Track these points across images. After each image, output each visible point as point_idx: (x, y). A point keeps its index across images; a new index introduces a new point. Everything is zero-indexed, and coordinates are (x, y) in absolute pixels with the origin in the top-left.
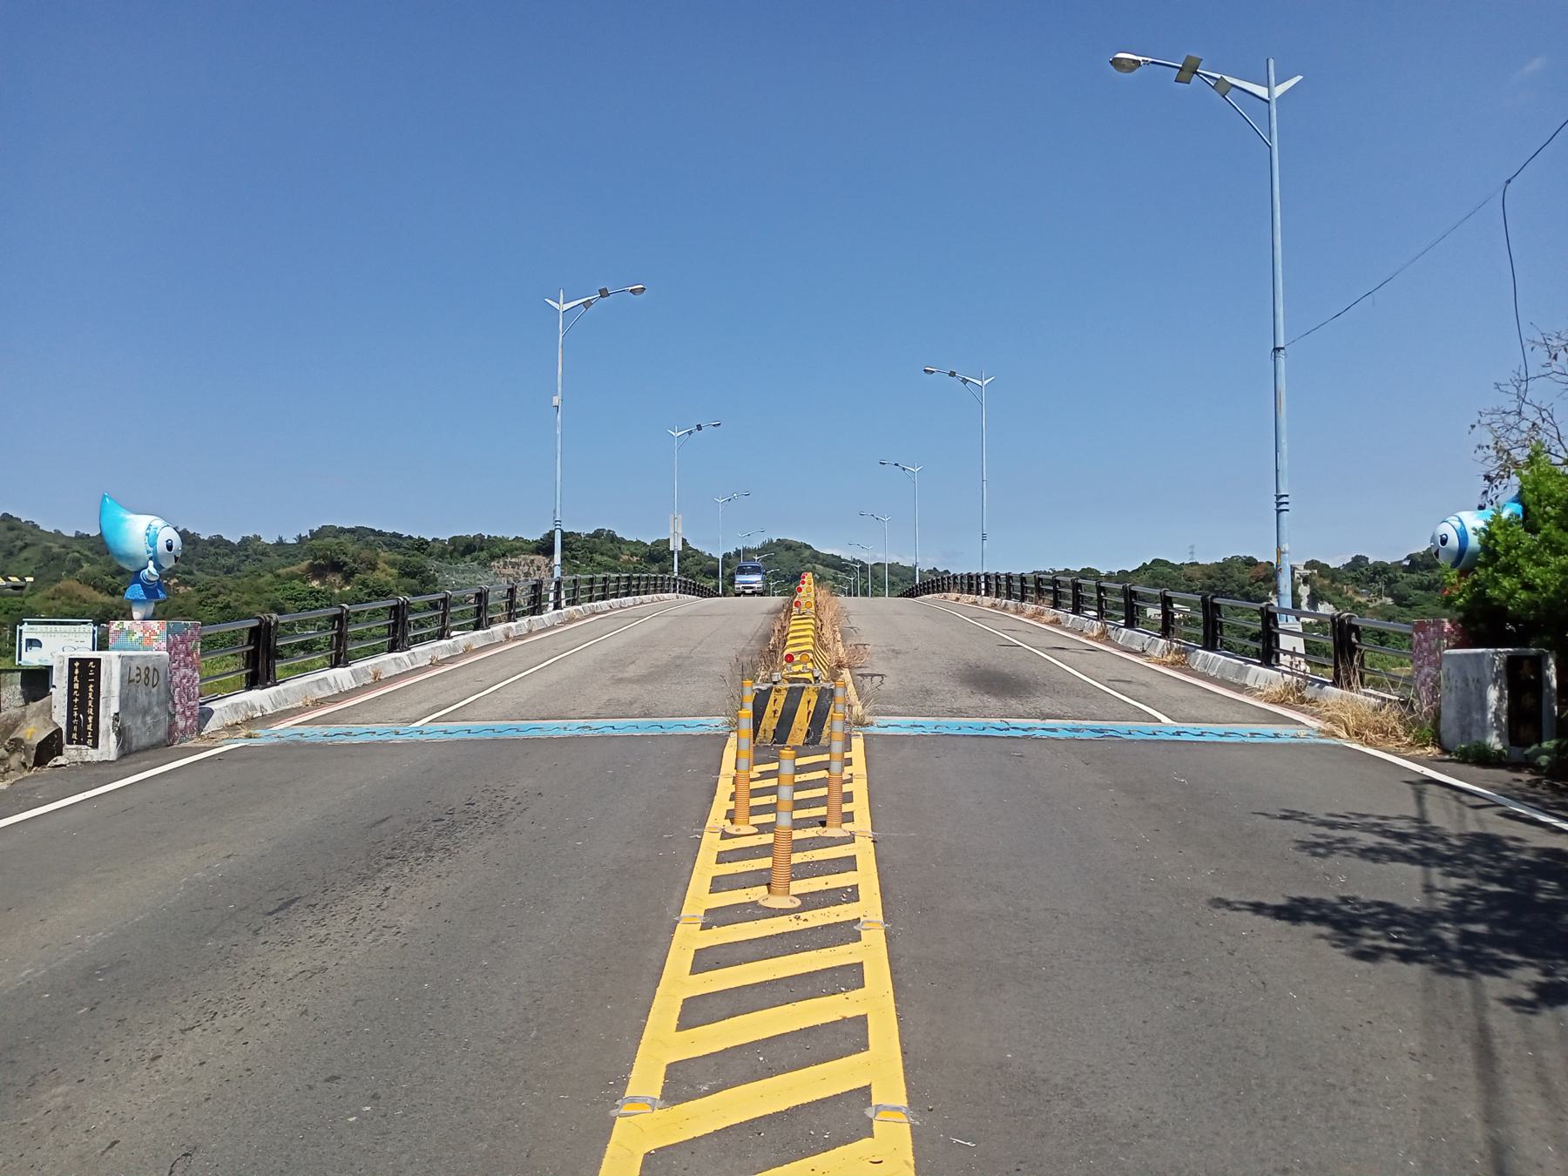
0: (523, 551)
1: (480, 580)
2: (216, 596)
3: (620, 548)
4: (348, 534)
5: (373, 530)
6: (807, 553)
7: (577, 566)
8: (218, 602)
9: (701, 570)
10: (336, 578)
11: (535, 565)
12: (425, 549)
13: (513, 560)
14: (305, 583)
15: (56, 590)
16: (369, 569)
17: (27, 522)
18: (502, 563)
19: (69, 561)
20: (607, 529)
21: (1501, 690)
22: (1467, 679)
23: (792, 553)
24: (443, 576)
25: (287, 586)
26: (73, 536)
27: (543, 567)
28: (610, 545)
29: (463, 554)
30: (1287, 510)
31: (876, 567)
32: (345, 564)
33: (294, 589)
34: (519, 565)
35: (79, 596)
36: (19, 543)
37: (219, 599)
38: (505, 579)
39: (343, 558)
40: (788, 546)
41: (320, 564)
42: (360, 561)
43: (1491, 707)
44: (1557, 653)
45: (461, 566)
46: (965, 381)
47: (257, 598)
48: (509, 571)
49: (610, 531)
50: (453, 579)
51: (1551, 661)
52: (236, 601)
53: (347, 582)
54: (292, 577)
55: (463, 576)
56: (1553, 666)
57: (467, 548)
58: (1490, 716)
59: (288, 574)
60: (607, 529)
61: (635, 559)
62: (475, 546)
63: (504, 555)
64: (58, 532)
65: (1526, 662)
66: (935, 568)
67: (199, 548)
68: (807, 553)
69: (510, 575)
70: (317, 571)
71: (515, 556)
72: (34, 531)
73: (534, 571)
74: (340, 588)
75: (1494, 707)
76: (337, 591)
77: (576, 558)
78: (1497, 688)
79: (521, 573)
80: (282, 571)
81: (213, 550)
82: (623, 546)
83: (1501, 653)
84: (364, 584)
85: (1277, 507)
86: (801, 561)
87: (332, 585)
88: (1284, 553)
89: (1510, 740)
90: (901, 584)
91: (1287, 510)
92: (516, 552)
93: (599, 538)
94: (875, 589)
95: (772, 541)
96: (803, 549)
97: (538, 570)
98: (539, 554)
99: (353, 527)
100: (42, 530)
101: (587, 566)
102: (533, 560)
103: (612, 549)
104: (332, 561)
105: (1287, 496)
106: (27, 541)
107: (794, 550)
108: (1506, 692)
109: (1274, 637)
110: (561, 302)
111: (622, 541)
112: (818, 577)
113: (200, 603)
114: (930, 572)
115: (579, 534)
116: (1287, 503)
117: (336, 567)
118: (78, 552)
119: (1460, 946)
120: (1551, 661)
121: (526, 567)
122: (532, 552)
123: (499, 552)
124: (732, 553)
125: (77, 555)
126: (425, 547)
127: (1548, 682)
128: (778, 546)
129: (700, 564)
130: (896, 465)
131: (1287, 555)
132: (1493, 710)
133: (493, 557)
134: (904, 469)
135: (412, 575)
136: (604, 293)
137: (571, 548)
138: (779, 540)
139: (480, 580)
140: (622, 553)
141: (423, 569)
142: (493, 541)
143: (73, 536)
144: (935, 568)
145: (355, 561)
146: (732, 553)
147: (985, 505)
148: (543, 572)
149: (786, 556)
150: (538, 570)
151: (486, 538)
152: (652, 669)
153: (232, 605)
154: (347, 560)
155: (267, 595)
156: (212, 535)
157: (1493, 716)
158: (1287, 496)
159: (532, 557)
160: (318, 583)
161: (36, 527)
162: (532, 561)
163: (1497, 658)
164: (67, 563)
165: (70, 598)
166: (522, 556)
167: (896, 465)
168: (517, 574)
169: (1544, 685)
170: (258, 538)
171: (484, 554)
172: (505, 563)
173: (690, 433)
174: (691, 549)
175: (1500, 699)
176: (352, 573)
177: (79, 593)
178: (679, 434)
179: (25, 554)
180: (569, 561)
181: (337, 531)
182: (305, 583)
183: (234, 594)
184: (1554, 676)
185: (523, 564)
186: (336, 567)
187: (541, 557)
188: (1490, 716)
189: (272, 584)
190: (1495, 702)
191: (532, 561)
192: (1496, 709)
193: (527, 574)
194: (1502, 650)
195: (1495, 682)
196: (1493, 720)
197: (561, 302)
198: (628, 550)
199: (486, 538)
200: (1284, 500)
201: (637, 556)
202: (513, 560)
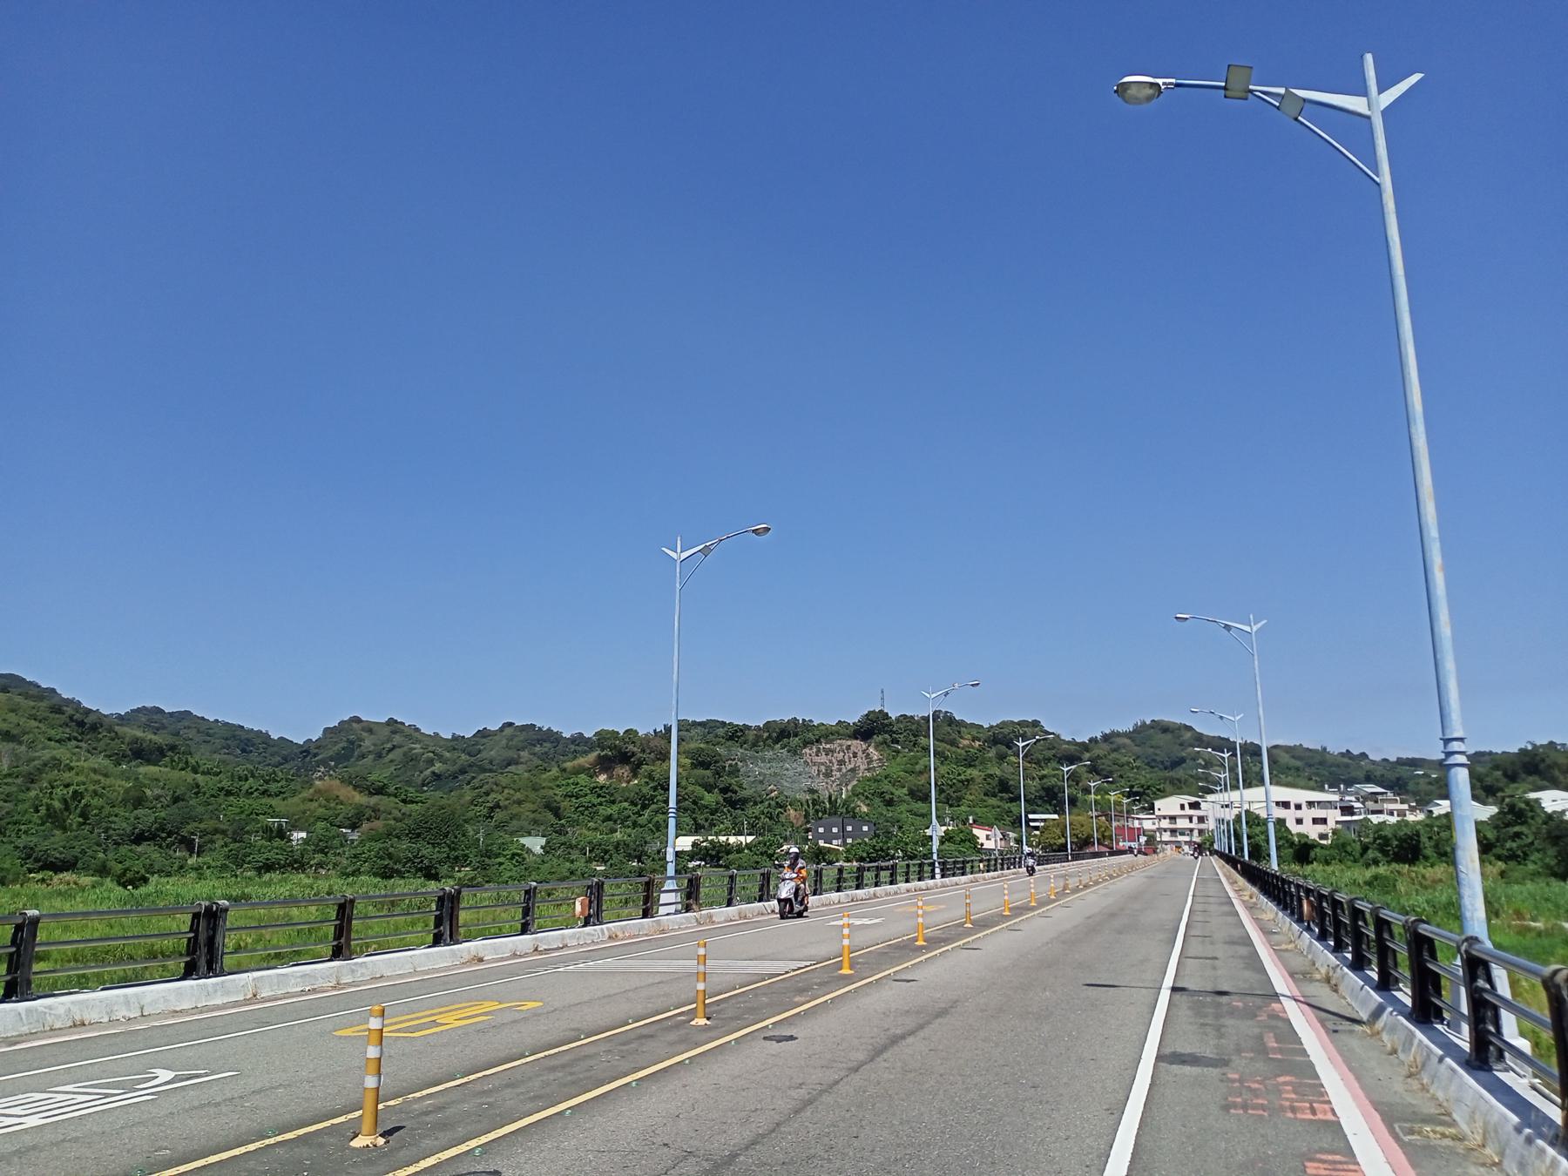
0: (840, 736)
1: (787, 770)
2: (487, 794)
3: (959, 732)
4: (699, 728)
6: (1188, 735)
7: (898, 752)
8: (488, 802)
9: (1054, 756)
10: (623, 771)
11: (851, 751)
12: (739, 737)
13: (828, 746)
14: (592, 777)
15: (315, 791)
16: (658, 759)
17: (409, 725)
18: (815, 750)
19: (424, 761)
20: (943, 711)
23: (1169, 736)
24: (747, 765)
25: (571, 781)
26: (450, 737)
27: (860, 753)
28: (949, 729)
29: (777, 741)
31: (1274, 751)
32: (633, 754)
33: (577, 784)
34: (833, 751)
35: (338, 797)
36: (389, 746)
37: (490, 798)
38: (816, 768)
39: (631, 747)
40: (1165, 728)
41: (606, 755)
42: (648, 751)
45: (769, 754)
47: (532, 795)
48: (823, 758)
49: (947, 712)
50: (756, 769)
52: (507, 799)
53: (635, 776)
54: (579, 771)
55: (769, 765)
57: (786, 735)
59: (574, 767)
60: (943, 711)
61: (977, 743)
62: (789, 732)
63: (818, 741)
64: (436, 734)
66: (1347, 751)
67: (560, 746)
68: (1188, 735)
69: (822, 764)
70: (605, 764)
71: (831, 742)
72: (416, 734)
73: (850, 758)
74: (628, 782)
76: (624, 785)
77: (897, 742)
79: (834, 761)
80: (568, 765)
81: (573, 747)
82: (962, 729)
84: (651, 777)
85: (1445, 747)
87: (620, 779)
90: (1307, 770)
92: (831, 737)
94: (1276, 776)
95: (1145, 723)
96: (1183, 732)
97: (854, 757)
98: (857, 739)
99: (705, 720)
100: (423, 733)
101: (910, 751)
102: (850, 746)
103: (949, 733)
104: (620, 751)
105: (1461, 739)
106: (395, 743)
107: (1172, 732)
111: (961, 724)
112: (1203, 763)
113: (472, 803)
114: (1342, 754)
115: (912, 717)
117: (624, 758)
118: (433, 752)
119: (1562, 984)
121: (842, 754)
122: (849, 736)
123: (813, 737)
125: (431, 755)
126: (739, 734)
128: (1153, 728)
129: (1054, 748)
133: (806, 743)
135: (705, 765)
137: (891, 731)
138: (1153, 721)
139: (787, 770)
140: (962, 738)
141: (718, 757)
142: (807, 726)
143: (450, 737)
144: (1347, 751)
145: (643, 751)
146: (1099, 737)
148: (860, 760)
150: (854, 757)
151: (801, 722)
152: (567, 1033)
153: (501, 804)
154: (635, 749)
155: (543, 792)
156: (574, 733)
158: (1461, 739)
159: (849, 743)
160: (605, 776)
161: (417, 730)
162: (849, 747)
164: (422, 764)
165: (327, 800)
166: (838, 741)
168: (831, 762)
170: (581, 734)
171: (795, 741)
172: (818, 750)
176: (640, 764)
177: (339, 794)
179: (391, 756)
180: (889, 746)
181: (689, 725)
182: (592, 777)
183: (506, 791)
185: (838, 749)
186: (624, 758)
187: (858, 742)
189: (556, 778)
191: (849, 747)
193: (842, 762)
197: (679, 550)
198: (969, 734)
199: (801, 722)
201: (979, 741)
202: (828, 746)
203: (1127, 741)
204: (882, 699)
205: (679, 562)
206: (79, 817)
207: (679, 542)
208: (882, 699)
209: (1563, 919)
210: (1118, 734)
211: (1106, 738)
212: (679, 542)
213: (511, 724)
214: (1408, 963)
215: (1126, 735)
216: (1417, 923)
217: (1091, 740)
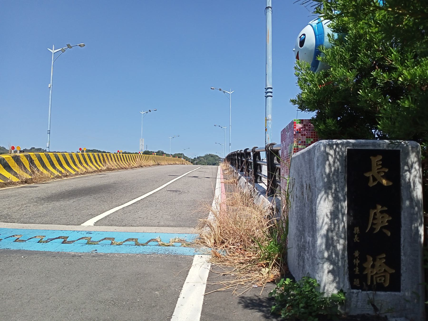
5: (98, 150)
21: (336, 199)
22: (302, 186)
23: (213, 158)
30: (271, 96)
40: (212, 156)
43: (321, 228)
44: (419, 233)
46: (224, 92)
51: (413, 158)
56: (416, 166)
58: (320, 241)
65: (376, 160)
75: (326, 227)
78: (330, 197)
83: (337, 145)
86: (215, 160)
88: (268, 120)
89: (352, 277)
91: (271, 96)
93: (159, 153)
105: (271, 88)
108: (345, 204)
109: (259, 167)
110: (53, 49)
116: (271, 92)
120: (413, 158)
124: (196, 158)
127: (409, 187)
128: (209, 156)
130: (219, 126)
131: (270, 121)
132: (323, 231)
134: (221, 127)
136: (69, 46)
146: (196, 158)
147: (230, 134)
149: (211, 158)
157: (324, 240)
158: (271, 88)
161: (5, 148)
163: (332, 152)
167: (219, 126)
169: (404, 193)
173: (147, 113)
174: (185, 156)
175: (334, 215)
178: (143, 113)
184: (417, 180)
188: (320, 241)
190: (327, 220)
192: (328, 231)
194: (339, 141)
195: (327, 187)
196: (324, 247)
197: (53, 49)
200: (269, 90)
203: (203, 159)
204: (147, 147)
205: (53, 53)
206: (367, 274)
207: (53, 47)
208: (147, 147)
209: (411, 189)
210: (201, 157)
211: (198, 158)
212: (53, 47)
213: (34, 148)
214: (402, 188)
215: (202, 157)
216: (254, 149)
217: (194, 158)
